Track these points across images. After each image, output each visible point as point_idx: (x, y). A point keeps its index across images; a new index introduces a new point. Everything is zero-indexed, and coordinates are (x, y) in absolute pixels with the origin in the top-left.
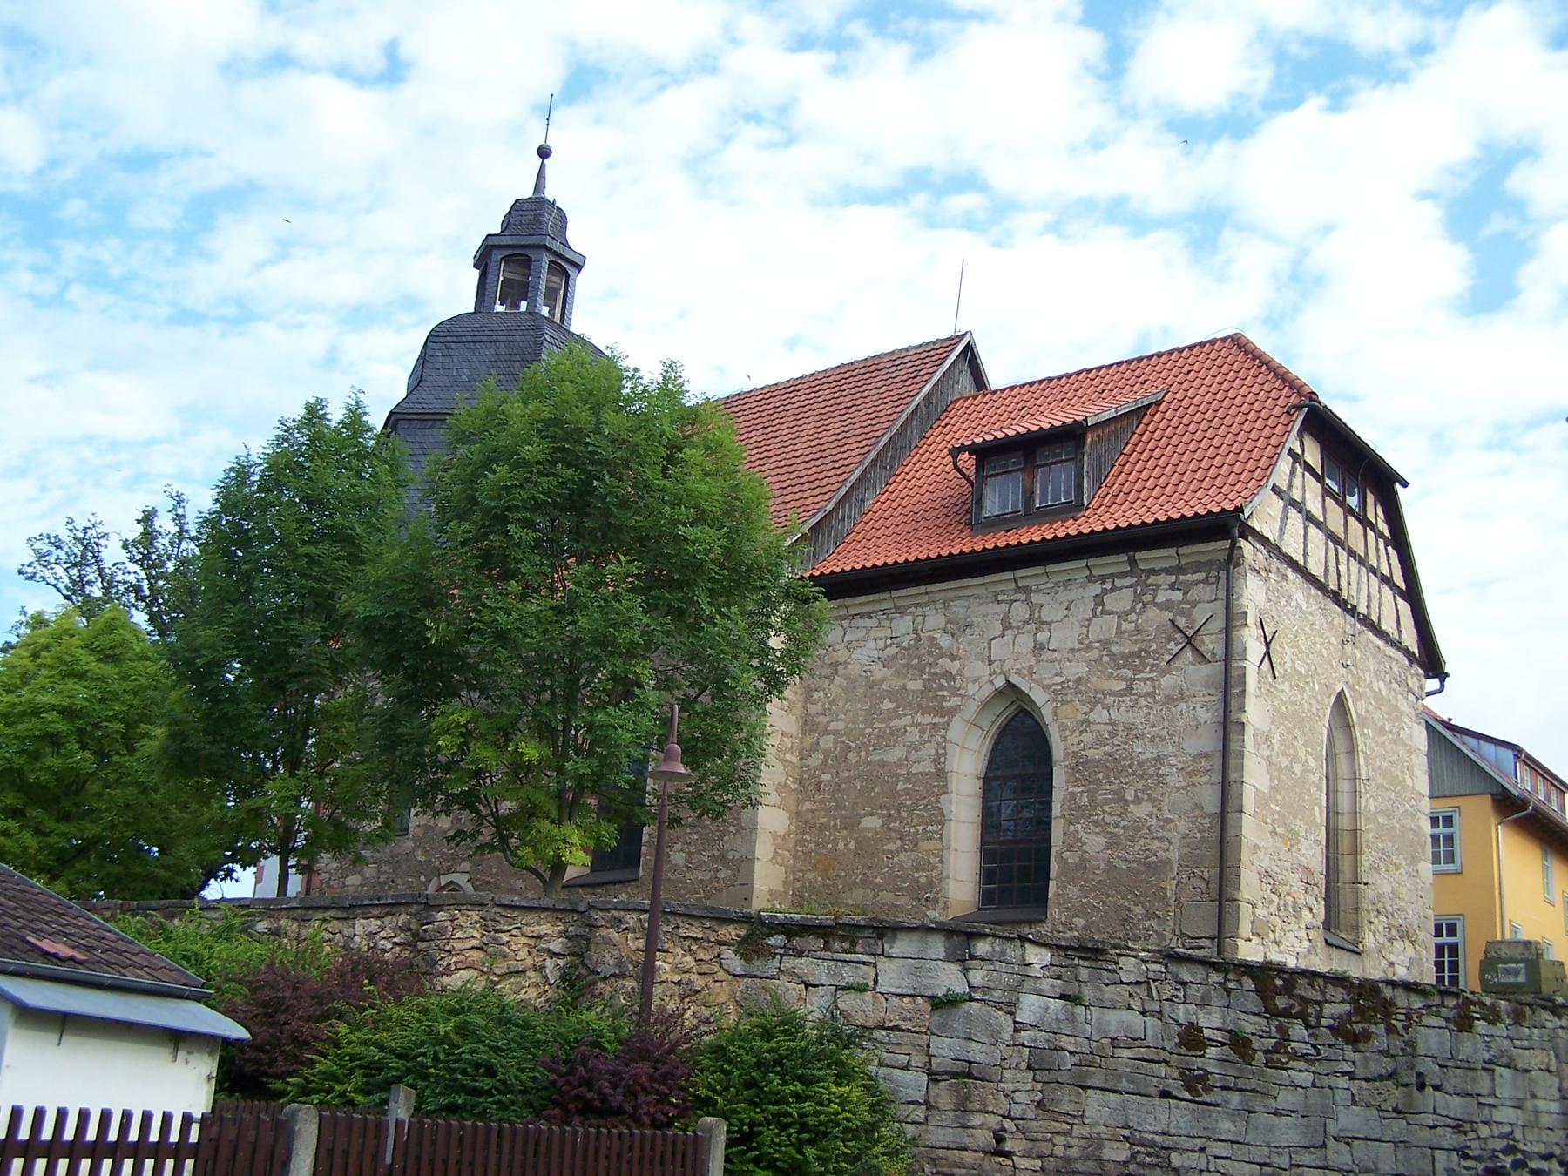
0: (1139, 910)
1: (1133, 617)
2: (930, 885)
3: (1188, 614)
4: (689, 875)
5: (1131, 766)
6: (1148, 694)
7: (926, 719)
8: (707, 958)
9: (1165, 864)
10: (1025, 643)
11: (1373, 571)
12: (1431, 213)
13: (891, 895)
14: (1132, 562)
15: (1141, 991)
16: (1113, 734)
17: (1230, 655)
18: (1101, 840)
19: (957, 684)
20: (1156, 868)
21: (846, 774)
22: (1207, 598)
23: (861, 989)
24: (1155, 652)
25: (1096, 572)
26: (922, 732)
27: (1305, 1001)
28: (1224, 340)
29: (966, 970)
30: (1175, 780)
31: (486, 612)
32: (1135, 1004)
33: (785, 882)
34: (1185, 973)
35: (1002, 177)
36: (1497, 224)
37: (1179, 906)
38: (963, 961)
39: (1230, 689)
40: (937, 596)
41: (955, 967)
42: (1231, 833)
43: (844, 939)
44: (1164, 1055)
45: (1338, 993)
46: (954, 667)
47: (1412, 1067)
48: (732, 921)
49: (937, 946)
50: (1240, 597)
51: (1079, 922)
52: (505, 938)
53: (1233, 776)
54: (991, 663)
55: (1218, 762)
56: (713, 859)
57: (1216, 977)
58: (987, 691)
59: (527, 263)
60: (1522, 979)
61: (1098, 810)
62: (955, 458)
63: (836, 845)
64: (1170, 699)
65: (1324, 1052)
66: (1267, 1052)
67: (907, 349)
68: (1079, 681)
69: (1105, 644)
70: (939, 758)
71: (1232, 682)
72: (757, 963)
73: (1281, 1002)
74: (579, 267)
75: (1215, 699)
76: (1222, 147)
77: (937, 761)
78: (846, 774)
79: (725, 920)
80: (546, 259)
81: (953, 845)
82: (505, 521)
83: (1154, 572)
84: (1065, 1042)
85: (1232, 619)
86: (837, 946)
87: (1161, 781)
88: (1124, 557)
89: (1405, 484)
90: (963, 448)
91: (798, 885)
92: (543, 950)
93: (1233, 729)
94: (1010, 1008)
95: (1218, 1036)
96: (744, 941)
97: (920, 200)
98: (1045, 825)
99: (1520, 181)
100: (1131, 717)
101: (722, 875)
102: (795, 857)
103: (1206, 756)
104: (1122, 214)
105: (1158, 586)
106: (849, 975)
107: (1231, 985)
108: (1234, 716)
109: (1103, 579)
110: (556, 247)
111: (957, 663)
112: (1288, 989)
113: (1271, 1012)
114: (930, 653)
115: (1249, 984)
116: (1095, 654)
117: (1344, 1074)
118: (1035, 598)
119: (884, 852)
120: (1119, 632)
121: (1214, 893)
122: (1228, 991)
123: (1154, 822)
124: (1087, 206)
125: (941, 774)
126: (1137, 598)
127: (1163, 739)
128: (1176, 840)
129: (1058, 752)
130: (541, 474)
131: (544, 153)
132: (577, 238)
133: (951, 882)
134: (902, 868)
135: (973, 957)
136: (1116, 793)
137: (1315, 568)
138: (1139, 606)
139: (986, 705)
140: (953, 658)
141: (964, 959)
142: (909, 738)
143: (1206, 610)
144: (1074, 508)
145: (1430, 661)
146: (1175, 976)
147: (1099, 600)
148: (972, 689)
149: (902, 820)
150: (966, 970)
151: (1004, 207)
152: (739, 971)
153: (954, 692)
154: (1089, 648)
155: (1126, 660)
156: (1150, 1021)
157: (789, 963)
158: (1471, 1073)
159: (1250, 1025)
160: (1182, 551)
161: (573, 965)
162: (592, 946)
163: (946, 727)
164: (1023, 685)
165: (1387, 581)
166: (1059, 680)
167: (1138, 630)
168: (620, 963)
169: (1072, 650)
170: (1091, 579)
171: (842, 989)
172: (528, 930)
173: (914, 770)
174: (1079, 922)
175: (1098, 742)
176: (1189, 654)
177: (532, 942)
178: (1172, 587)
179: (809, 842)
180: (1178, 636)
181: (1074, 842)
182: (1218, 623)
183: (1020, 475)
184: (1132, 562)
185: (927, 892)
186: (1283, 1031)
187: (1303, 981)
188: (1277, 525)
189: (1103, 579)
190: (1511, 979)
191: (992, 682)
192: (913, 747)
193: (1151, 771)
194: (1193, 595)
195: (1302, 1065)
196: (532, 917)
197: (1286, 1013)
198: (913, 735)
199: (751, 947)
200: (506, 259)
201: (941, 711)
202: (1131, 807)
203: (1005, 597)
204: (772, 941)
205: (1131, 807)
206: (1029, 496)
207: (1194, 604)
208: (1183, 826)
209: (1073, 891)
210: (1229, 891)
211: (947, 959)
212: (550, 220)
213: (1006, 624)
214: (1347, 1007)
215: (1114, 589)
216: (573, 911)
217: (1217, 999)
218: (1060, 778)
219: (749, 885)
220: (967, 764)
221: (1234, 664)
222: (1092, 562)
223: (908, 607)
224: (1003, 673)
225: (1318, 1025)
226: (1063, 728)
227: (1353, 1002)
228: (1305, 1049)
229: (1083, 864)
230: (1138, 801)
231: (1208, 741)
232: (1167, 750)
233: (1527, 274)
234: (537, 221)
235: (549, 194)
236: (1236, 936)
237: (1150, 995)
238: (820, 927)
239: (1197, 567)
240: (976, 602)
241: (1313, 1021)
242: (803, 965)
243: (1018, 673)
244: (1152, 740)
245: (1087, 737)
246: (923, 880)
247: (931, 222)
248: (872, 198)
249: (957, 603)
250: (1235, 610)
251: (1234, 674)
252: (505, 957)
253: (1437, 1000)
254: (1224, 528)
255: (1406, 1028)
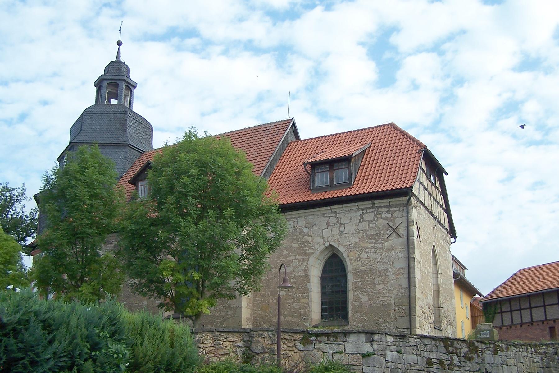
0: (381, 320)
1: (374, 222)
2: (305, 314)
3: (393, 221)
4: (216, 313)
5: (376, 272)
6: (380, 248)
7: (300, 257)
8: (291, 345)
9: (391, 304)
10: (336, 231)
11: (438, 203)
12: (362, 51)
13: (291, 318)
14: (373, 204)
15: (415, 348)
16: (369, 262)
17: (409, 235)
18: (367, 297)
19: (311, 245)
20: (386, 306)
21: (271, 276)
22: (400, 216)
23: (340, 353)
24: (383, 234)
25: (360, 207)
26: (299, 262)
27: (457, 348)
28: (388, 125)
29: (372, 345)
30: (392, 277)
31: (182, 228)
32: (414, 352)
33: (251, 315)
34: (426, 342)
35: (206, 32)
36: (387, 55)
37: (395, 319)
38: (370, 342)
39: (409, 247)
40: (301, 215)
41: (368, 344)
42: (412, 294)
43: (333, 337)
44: (423, 368)
45: (464, 345)
46: (310, 239)
47: (484, 367)
48: (299, 333)
49: (363, 338)
50: (411, 215)
51: (360, 325)
52: (221, 342)
53: (411, 275)
54: (323, 238)
55: (406, 271)
56: (226, 308)
57: (434, 342)
58: (322, 247)
59: (117, 86)
60: (488, 336)
61: (365, 287)
62: (305, 166)
63: (268, 301)
64: (388, 250)
65: (463, 364)
66: (448, 365)
67: (270, 124)
68: (356, 244)
69: (365, 231)
70: (306, 270)
71: (410, 244)
72: (307, 346)
73: (451, 349)
74: (135, 87)
75: (404, 249)
76: (287, 23)
77: (305, 271)
78: (271, 276)
79: (296, 333)
80: (124, 84)
81: (313, 300)
82: (186, 196)
83: (381, 207)
84: (399, 366)
85: (409, 223)
86: (332, 339)
87: (387, 277)
88: (370, 202)
89: (447, 174)
90: (308, 163)
91: (255, 315)
92: (235, 346)
93: (411, 260)
94: (384, 356)
95: (436, 361)
96: (302, 339)
97: (175, 40)
98: (344, 292)
99: (394, 39)
100: (376, 256)
101: (229, 313)
102: (253, 306)
103: (402, 268)
104: (251, 47)
105: (382, 212)
106: (336, 348)
107: (438, 345)
108: (411, 256)
109: (363, 209)
110: (128, 80)
111: (310, 238)
112: (452, 345)
113: (449, 353)
114: (300, 234)
115: (442, 344)
116: (361, 235)
117: (468, 370)
118: (338, 215)
119: (287, 303)
120: (369, 227)
121: (408, 313)
122: (437, 346)
123: (385, 291)
124: (236, 44)
125: (307, 276)
126: (375, 216)
127: (387, 263)
128: (393, 296)
129: (349, 267)
130: (197, 180)
131: (119, 43)
132: (134, 76)
133: (313, 313)
134: (294, 308)
135: (374, 341)
136: (371, 281)
137: (427, 205)
138: (376, 219)
139: (322, 252)
140: (309, 236)
141: (371, 342)
142: (294, 264)
143: (400, 220)
144: (349, 184)
145: (452, 232)
146: (424, 343)
147: (361, 217)
148: (317, 247)
149: (293, 292)
150: (372, 345)
151: (208, 43)
152: (302, 349)
153: (310, 248)
154: (359, 233)
155: (370, 237)
156: (419, 357)
157: (317, 345)
158: (498, 368)
159: (443, 357)
160: (391, 200)
161: (246, 350)
162: (253, 344)
163: (308, 260)
164: (336, 245)
165: (441, 206)
166: (349, 243)
167: (376, 226)
168: (263, 349)
169: (353, 233)
170: (358, 209)
171: (335, 353)
172: (230, 339)
173: (296, 275)
174: (360, 325)
175: (364, 264)
176: (394, 235)
177: (231, 343)
178: (387, 212)
179: (259, 300)
180: (390, 229)
181: (357, 298)
182: (404, 224)
183: (328, 173)
184: (373, 204)
185: (304, 317)
186: (452, 358)
187: (455, 342)
188: (418, 191)
189: (363, 209)
190: (485, 336)
191: (324, 244)
192: (296, 267)
193: (383, 274)
194: (395, 215)
195: (457, 368)
196: (230, 335)
197: (452, 353)
198: (296, 263)
199: (305, 341)
200: (108, 84)
201: (305, 254)
202: (377, 286)
203: (327, 215)
204: (311, 339)
205: (377, 286)
206: (332, 180)
207: (395, 218)
208: (395, 292)
209: (358, 315)
210: (412, 313)
211: (366, 342)
212: (124, 69)
213: (328, 224)
214: (467, 349)
215: (367, 213)
216: (245, 332)
217: (434, 349)
218: (350, 277)
219: (240, 316)
220: (315, 273)
221: (410, 238)
222: (359, 204)
223: (291, 218)
224: (328, 241)
225: (461, 356)
226: (351, 260)
227: (468, 348)
228: (458, 363)
229: (361, 305)
230: (379, 284)
231: (403, 264)
232: (388, 267)
233: (399, 74)
234: (119, 70)
235: (122, 59)
236: (416, 328)
237: (418, 349)
238: (326, 333)
239: (396, 206)
240: (316, 216)
241: (459, 354)
242: (322, 346)
243: (334, 241)
244: (383, 263)
245: (360, 263)
246: (302, 313)
247: (179, 49)
248: (154, 38)
249: (310, 217)
250: (410, 220)
251: (411, 241)
252: (222, 348)
253: (488, 346)
254: (406, 192)
255: (482, 355)
